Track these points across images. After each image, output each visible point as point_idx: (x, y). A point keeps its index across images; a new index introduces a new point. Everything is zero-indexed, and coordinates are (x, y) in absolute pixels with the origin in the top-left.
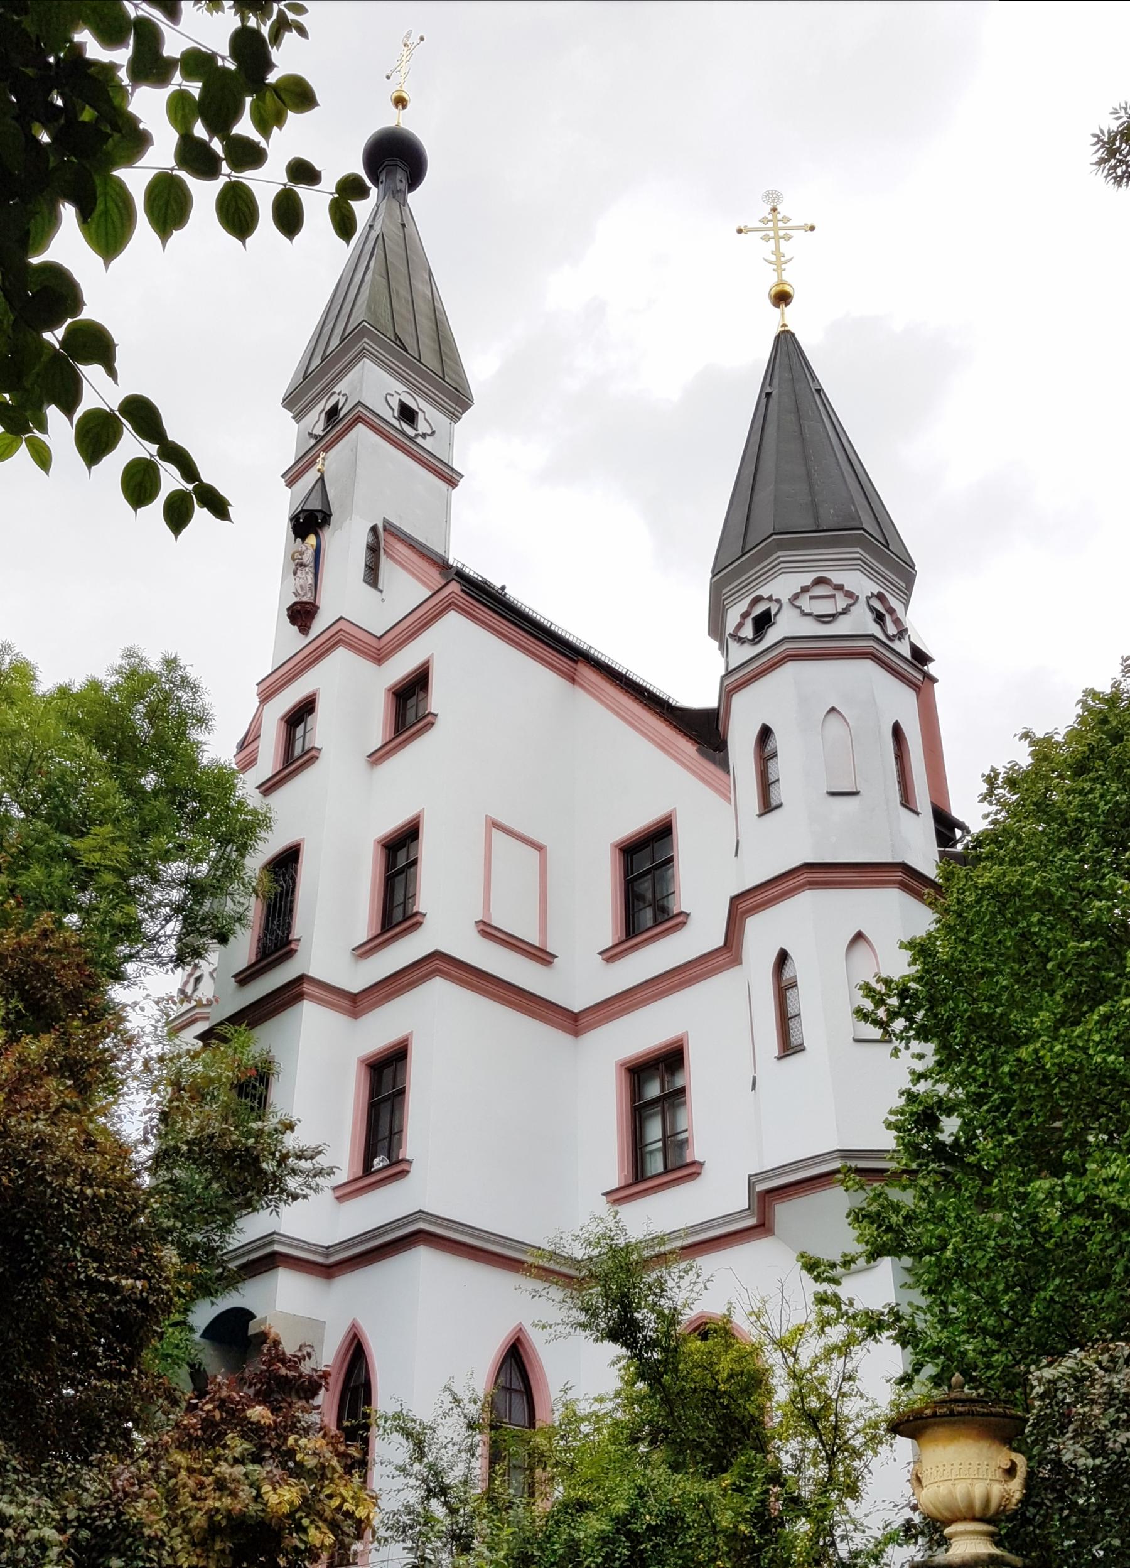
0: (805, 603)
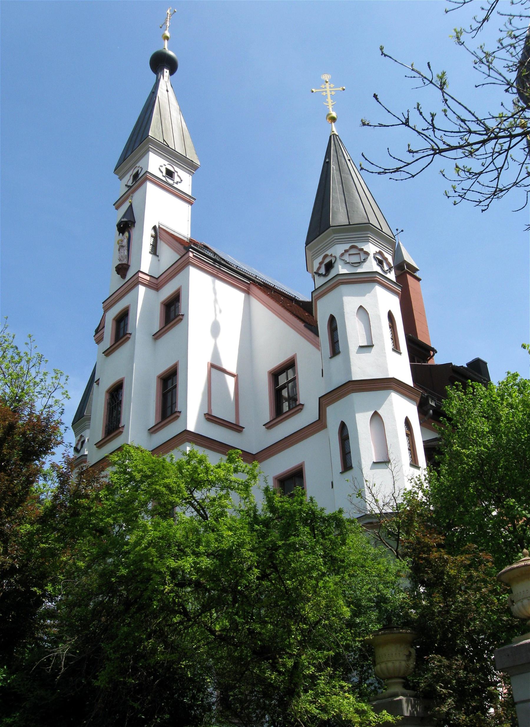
0: (346, 258)
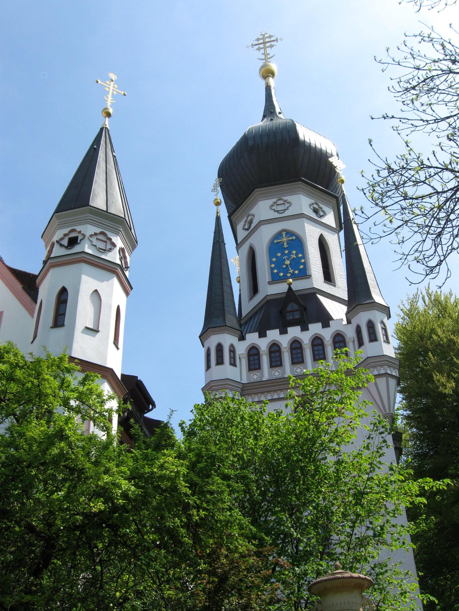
0: (94, 239)
